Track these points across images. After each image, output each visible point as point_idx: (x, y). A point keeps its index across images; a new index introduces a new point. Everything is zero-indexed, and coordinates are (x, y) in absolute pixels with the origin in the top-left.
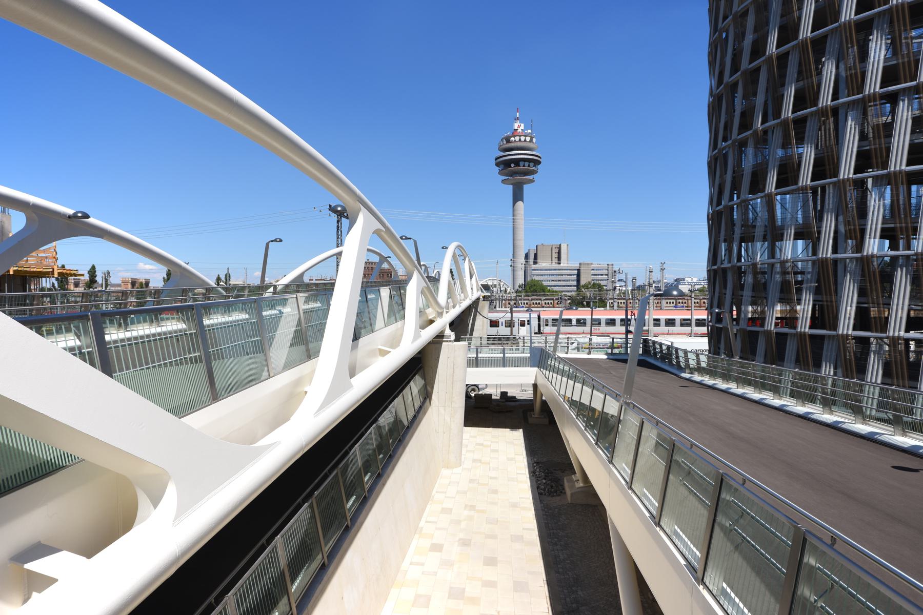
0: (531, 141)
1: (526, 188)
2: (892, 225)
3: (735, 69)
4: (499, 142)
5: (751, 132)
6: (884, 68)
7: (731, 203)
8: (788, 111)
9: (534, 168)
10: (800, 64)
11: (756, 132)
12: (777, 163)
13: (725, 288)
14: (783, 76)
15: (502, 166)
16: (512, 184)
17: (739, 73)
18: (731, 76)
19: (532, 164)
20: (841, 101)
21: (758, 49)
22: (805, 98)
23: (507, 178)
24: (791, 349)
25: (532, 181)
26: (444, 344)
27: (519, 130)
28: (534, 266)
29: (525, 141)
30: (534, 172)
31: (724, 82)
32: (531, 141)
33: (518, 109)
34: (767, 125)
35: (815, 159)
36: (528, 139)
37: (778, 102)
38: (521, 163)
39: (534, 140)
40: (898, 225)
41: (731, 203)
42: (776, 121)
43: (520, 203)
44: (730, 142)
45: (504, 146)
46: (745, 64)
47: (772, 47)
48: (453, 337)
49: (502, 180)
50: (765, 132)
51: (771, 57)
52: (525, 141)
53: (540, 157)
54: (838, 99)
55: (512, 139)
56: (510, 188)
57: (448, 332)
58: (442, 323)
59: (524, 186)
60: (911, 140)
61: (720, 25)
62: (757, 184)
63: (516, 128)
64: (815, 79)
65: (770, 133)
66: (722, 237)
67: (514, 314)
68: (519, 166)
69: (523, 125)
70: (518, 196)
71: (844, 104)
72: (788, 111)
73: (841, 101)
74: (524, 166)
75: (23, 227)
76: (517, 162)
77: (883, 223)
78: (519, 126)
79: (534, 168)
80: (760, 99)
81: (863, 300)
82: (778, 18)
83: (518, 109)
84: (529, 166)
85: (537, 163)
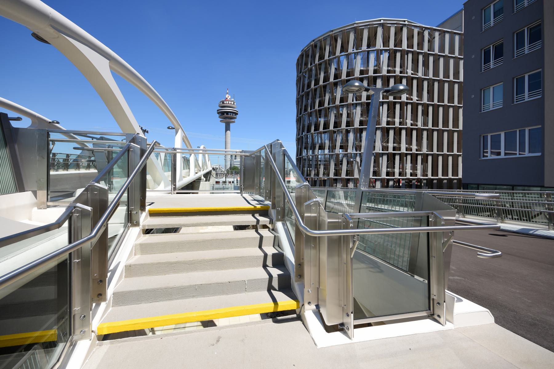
0: (234, 104)
1: (232, 125)
2: (342, 145)
3: (303, 91)
4: (218, 103)
5: (307, 112)
6: (340, 97)
7: (302, 135)
8: (317, 107)
9: (235, 116)
10: (320, 94)
11: (308, 112)
12: (314, 123)
13: (301, 165)
14: (315, 94)
15: (220, 114)
16: (225, 123)
17: (304, 92)
18: (302, 93)
19: (234, 114)
20: (330, 106)
21: (309, 86)
22: (321, 104)
23: (222, 119)
24: (318, 183)
25: (234, 122)
26: (201, 182)
27: (228, 99)
28: (235, 160)
29: (231, 103)
30: (235, 118)
31: (305, 91)
32: (234, 104)
33: (228, 89)
34: (311, 110)
35: (324, 123)
36: (232, 103)
37: (314, 103)
38: (229, 114)
39: (235, 104)
40: (344, 145)
41: (302, 135)
42: (314, 110)
43: (228, 132)
44: (301, 115)
45: (221, 105)
46: (305, 90)
47: (313, 86)
48: (205, 179)
49: (220, 121)
50: (311, 113)
51: (312, 89)
52: (231, 103)
53: (238, 112)
54: (329, 105)
55: (225, 102)
57: (203, 178)
58: (202, 173)
59: (231, 124)
60: (347, 120)
61: (303, 71)
62: (309, 130)
63: (227, 97)
64: (324, 98)
65: (312, 113)
66: (304, 147)
67: (227, 179)
68: (228, 115)
69: (230, 96)
70: (227, 128)
71: (331, 107)
72: (317, 107)
73: (330, 106)
74: (230, 115)
75: (13, 126)
76: (227, 113)
77: (340, 144)
78: (228, 97)
79: (235, 116)
80: (310, 101)
81: (336, 167)
82: (314, 77)
83: (228, 89)
84: (233, 115)
85: (236, 114)
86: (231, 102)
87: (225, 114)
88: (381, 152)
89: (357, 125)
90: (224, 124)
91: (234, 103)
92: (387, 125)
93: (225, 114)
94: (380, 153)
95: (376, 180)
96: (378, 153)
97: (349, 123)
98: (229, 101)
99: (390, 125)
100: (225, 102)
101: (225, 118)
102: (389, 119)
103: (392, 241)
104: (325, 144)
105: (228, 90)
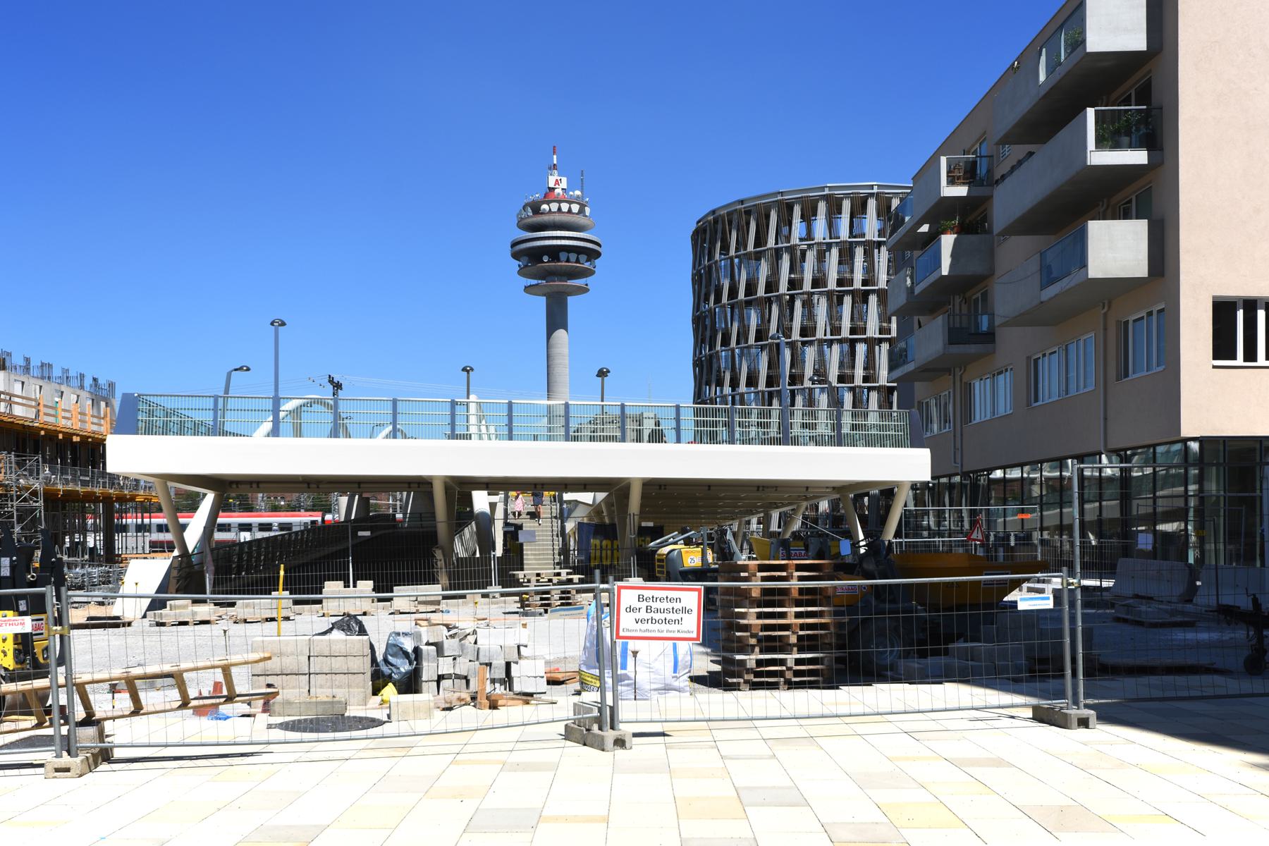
0: (581, 211)
16: (544, 295)
19: (583, 258)
23: (534, 282)
25: (584, 290)
27: (558, 191)
29: (570, 211)
30: (588, 273)
32: (581, 211)
36: (575, 208)
38: (563, 256)
39: (587, 210)
43: (560, 334)
45: (530, 220)
52: (570, 211)
55: (545, 207)
56: (539, 304)
63: (551, 185)
68: (559, 260)
69: (564, 180)
70: (556, 319)
74: (568, 261)
76: (554, 252)
84: (578, 261)
85: (593, 255)
86: (570, 203)
87: (545, 259)
88: (877, 336)
89: (832, 285)
90: (542, 301)
91: (582, 207)
92: (862, 286)
93: (545, 259)
94: (875, 339)
95: (870, 389)
96: (872, 337)
97: (771, 286)
98: (560, 202)
99: (845, 287)
100: (545, 207)
101: (547, 275)
102: (793, 276)
103: (1176, 690)
104: (749, 328)
105: (554, 153)
